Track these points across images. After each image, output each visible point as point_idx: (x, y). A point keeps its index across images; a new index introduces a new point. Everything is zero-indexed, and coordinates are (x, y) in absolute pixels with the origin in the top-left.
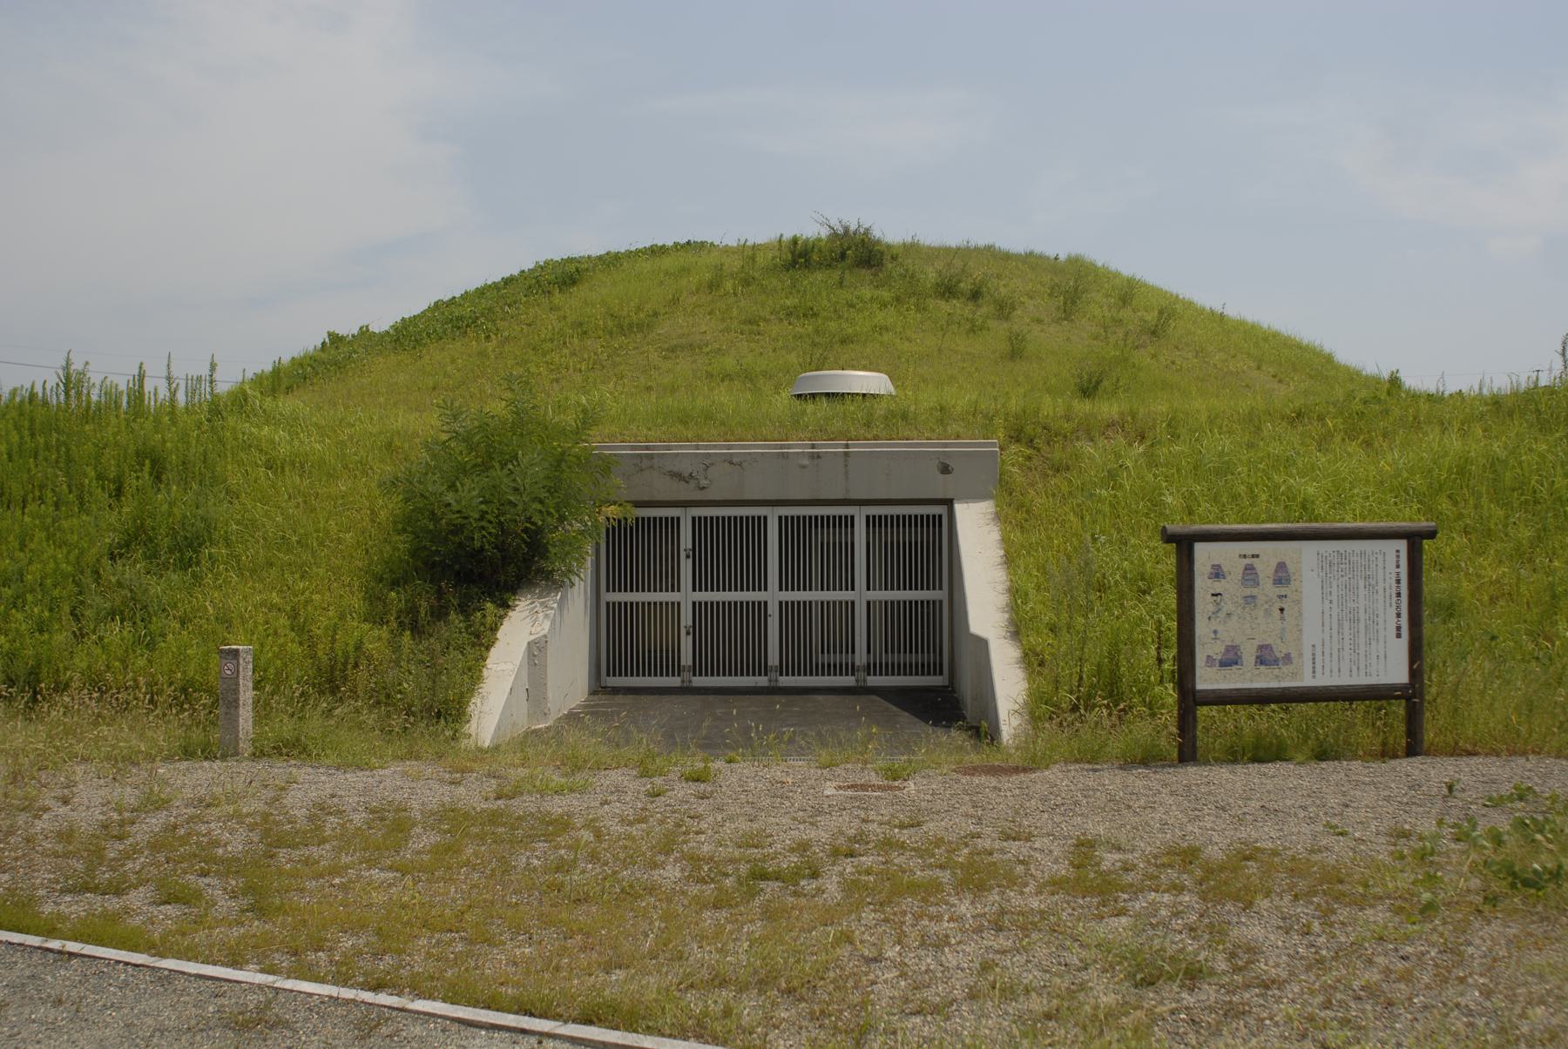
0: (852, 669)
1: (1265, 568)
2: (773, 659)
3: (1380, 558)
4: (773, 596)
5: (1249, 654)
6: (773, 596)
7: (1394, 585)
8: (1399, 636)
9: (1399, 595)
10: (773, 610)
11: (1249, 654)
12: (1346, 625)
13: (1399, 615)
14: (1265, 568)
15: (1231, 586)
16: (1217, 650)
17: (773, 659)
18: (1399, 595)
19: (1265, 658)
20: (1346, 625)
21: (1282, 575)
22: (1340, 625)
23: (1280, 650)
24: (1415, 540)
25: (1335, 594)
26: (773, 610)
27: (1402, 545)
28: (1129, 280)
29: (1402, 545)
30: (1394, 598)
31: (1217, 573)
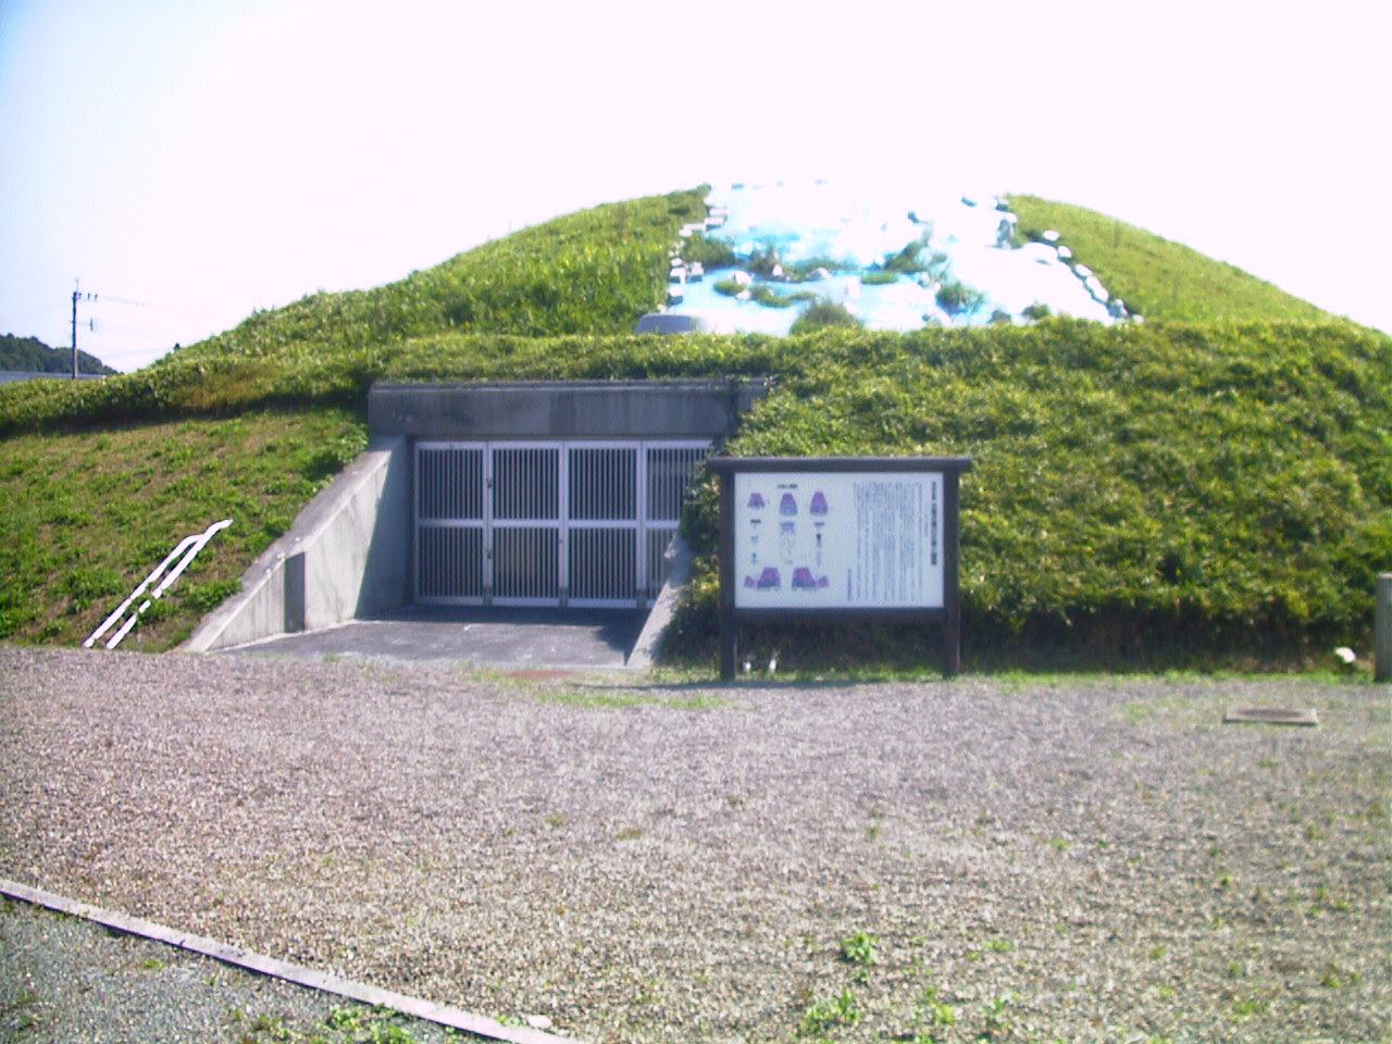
0: (553, 590)
1: (803, 498)
2: (564, 581)
3: (917, 490)
4: (563, 523)
5: (786, 576)
6: (563, 523)
7: (930, 516)
8: (934, 562)
9: (934, 524)
10: (564, 536)
11: (786, 576)
12: (882, 553)
13: (934, 544)
14: (803, 498)
15: (771, 514)
16: (756, 572)
17: (564, 581)
18: (934, 524)
19: (802, 579)
20: (882, 553)
21: (819, 504)
22: (876, 550)
23: (816, 573)
24: (951, 472)
25: (871, 522)
26: (564, 536)
27: (938, 478)
28: (619, 204)
29: (938, 478)
30: (930, 528)
31: (757, 501)
